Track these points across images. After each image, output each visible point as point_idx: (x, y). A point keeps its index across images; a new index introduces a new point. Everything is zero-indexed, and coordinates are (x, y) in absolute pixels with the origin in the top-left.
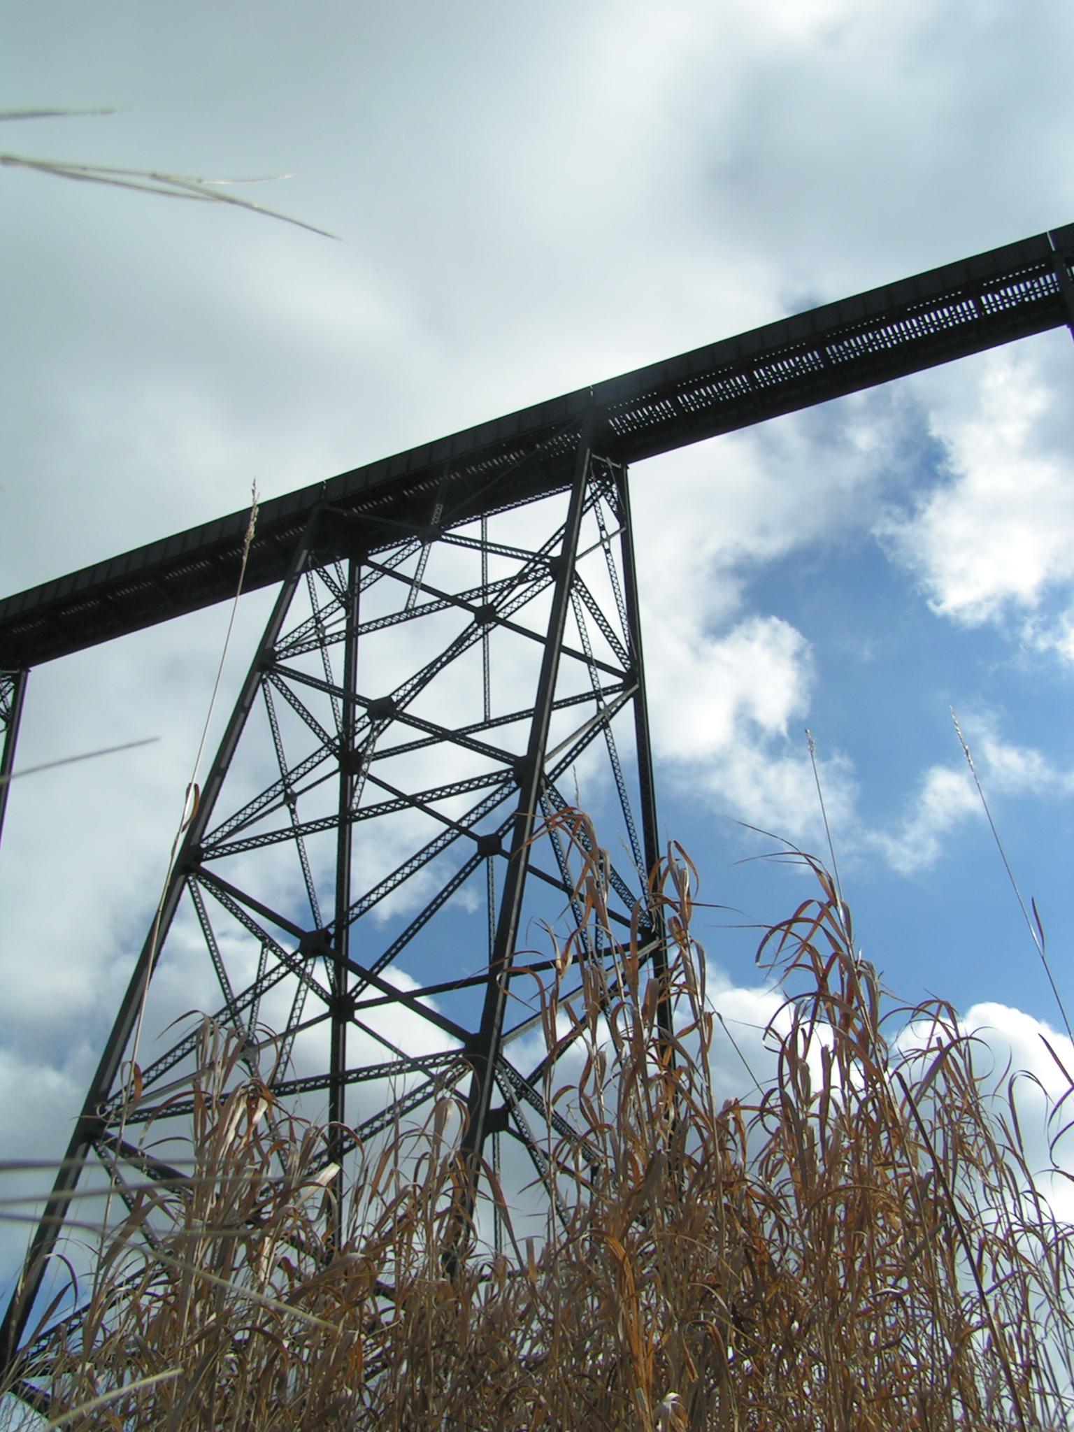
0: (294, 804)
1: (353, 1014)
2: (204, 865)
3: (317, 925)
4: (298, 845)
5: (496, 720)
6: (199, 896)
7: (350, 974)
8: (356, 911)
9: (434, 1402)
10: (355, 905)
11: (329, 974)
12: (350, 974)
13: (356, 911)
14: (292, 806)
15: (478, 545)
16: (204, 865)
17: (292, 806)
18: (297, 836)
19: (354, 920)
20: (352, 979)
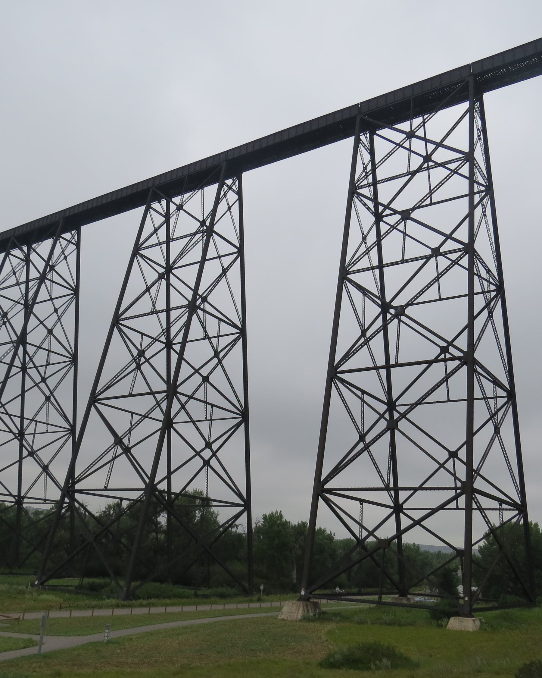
0: (231, 210)
1: (16, 501)
2: (348, 276)
3: (218, 254)
4: (220, 260)
5: (407, 260)
6: (124, 318)
7: (380, 206)
8: (172, 324)
9: (115, 597)
10: (172, 323)
11: (238, 241)
12: (380, 206)
13: (172, 324)
14: (230, 210)
15: (11, 342)
16: (348, 276)
17: (230, 210)
18: (159, 245)
19: (172, 326)
20: (381, 208)
